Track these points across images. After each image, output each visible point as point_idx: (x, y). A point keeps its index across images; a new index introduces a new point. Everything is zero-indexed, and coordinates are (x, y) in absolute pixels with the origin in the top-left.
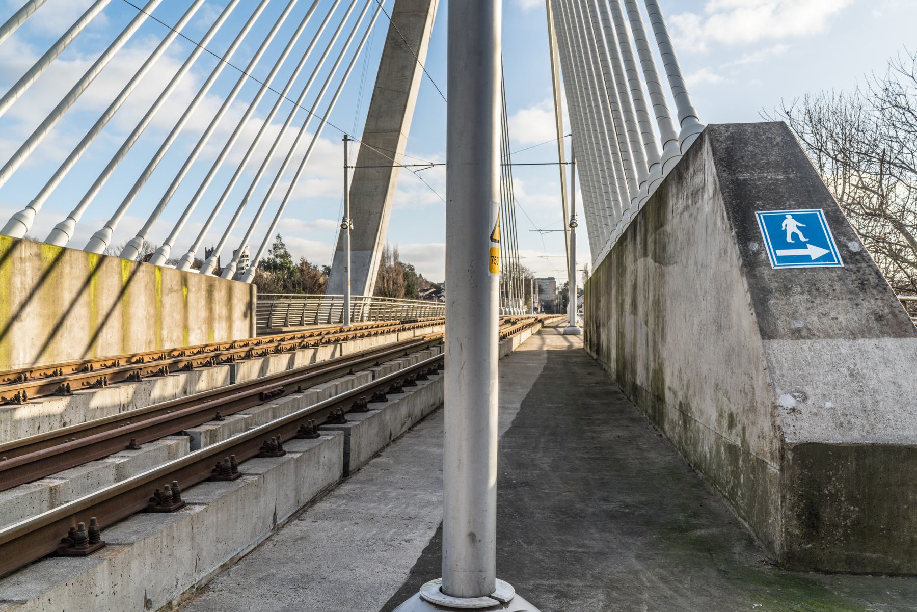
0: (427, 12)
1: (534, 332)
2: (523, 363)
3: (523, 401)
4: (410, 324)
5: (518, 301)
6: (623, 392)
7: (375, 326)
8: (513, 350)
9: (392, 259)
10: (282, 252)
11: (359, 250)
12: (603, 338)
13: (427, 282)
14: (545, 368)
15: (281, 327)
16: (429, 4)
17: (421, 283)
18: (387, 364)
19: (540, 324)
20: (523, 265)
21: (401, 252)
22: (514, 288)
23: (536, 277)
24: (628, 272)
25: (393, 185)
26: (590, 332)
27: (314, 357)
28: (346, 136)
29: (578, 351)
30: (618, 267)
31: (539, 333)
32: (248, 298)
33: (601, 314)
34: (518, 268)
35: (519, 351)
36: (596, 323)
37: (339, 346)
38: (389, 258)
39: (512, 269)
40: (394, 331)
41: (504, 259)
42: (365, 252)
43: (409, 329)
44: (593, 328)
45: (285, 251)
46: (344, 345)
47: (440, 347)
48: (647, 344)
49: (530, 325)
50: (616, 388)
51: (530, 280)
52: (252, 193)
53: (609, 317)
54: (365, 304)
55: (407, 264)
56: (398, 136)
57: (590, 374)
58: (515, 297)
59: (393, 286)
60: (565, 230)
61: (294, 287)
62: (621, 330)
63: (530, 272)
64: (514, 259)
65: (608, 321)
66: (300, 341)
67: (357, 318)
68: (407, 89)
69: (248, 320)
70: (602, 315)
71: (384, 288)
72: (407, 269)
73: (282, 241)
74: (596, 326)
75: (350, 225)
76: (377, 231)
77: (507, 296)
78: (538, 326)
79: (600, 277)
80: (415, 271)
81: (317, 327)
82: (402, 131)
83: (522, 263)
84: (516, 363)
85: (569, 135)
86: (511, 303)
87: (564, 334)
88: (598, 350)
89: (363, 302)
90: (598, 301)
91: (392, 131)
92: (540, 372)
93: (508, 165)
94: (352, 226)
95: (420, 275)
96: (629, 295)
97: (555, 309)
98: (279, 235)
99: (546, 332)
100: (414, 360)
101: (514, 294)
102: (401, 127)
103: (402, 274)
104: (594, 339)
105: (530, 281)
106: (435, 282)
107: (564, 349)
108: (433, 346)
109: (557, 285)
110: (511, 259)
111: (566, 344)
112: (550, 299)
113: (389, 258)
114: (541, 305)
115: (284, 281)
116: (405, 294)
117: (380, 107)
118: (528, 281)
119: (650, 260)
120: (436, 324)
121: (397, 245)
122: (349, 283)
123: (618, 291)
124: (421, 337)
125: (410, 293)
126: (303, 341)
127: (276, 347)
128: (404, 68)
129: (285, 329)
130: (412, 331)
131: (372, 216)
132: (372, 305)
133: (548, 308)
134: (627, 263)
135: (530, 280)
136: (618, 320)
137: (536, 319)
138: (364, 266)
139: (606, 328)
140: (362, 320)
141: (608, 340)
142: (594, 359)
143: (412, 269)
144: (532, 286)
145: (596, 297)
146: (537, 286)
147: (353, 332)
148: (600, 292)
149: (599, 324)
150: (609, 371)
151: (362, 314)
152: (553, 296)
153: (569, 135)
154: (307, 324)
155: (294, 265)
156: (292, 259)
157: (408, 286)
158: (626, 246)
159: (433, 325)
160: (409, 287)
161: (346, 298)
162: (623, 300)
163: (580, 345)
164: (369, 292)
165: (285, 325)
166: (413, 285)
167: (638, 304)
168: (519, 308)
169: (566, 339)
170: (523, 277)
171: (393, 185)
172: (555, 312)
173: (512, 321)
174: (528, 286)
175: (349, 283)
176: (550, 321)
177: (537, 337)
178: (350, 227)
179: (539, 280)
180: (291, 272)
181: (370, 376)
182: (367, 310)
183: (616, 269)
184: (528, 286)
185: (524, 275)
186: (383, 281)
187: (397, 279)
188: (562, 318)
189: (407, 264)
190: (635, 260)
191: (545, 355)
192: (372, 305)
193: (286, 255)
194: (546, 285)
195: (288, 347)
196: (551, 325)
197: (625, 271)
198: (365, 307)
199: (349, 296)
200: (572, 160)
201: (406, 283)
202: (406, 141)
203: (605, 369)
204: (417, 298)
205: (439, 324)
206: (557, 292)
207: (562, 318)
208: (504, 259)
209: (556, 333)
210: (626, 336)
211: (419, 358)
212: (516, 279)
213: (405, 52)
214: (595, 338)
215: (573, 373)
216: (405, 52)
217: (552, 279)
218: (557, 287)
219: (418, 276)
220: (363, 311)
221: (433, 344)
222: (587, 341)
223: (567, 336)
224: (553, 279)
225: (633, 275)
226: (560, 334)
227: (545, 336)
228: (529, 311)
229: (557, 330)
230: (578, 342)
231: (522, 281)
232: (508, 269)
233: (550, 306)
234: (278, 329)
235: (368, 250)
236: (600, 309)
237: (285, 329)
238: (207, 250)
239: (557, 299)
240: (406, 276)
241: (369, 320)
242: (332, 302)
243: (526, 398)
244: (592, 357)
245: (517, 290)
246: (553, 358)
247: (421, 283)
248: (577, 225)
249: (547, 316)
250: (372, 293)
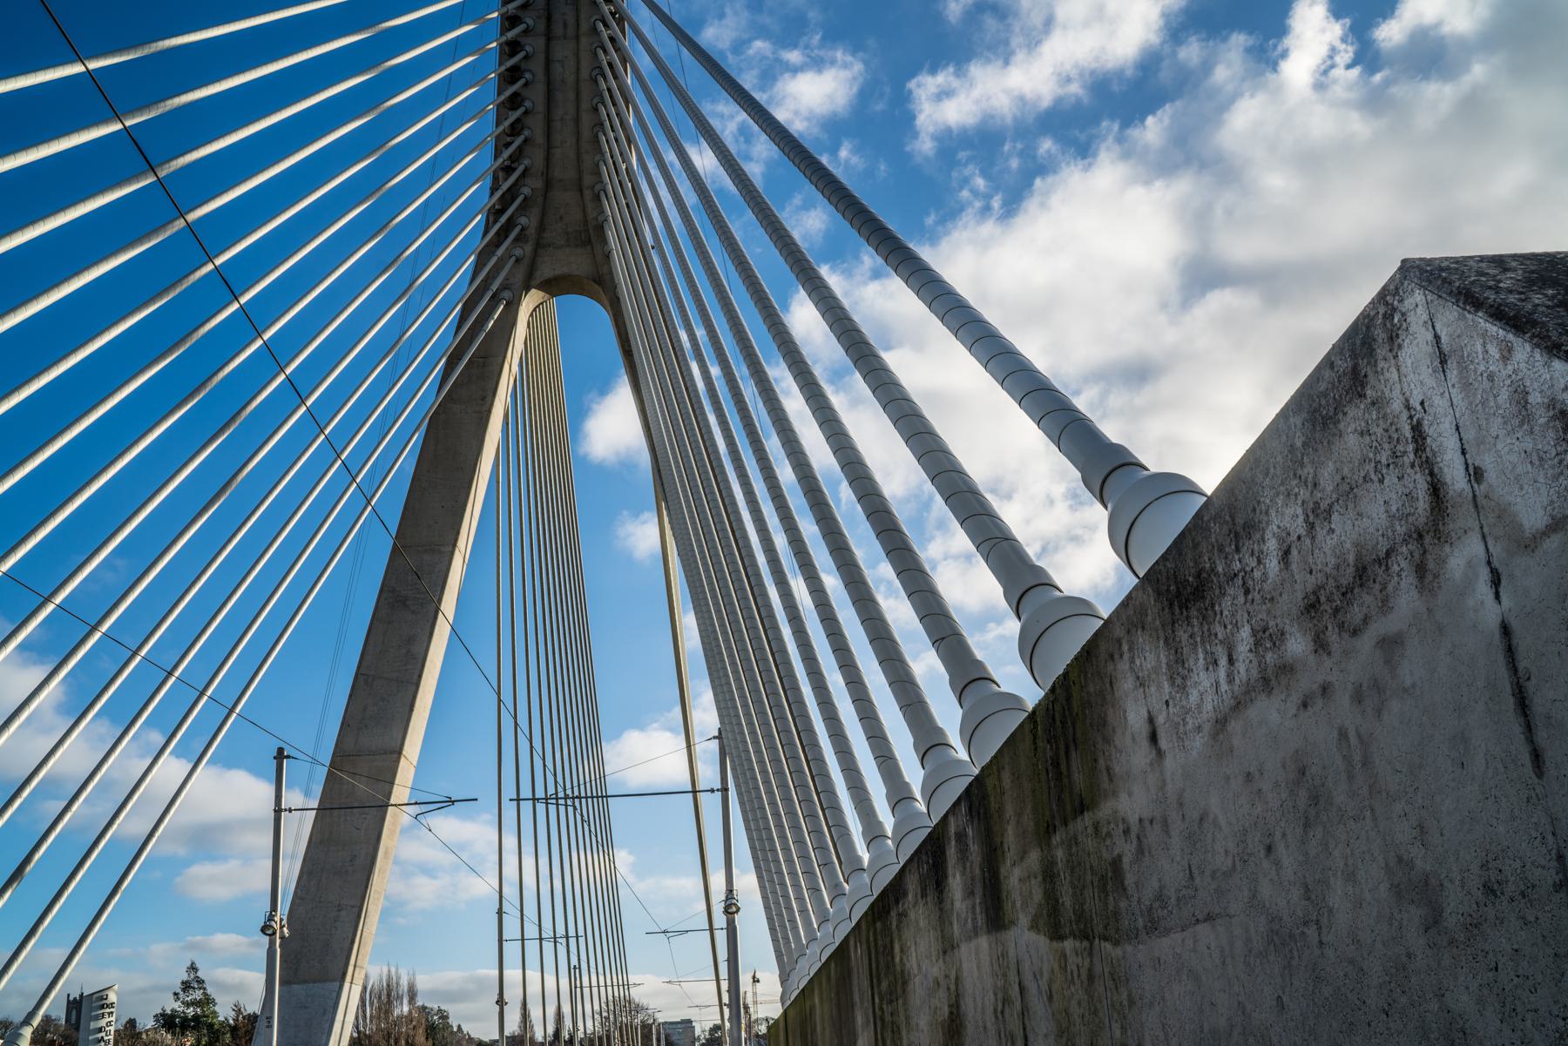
9: (405, 1001)
10: (198, 995)
20: (637, 1000)
23: (661, 1020)
24: (918, 988)
25: (386, 853)
28: (280, 750)
30: (875, 979)
34: (630, 1006)
39: (618, 1008)
41: (603, 989)
45: (205, 994)
51: (650, 1026)
55: (436, 1007)
56: (398, 761)
60: (711, 930)
63: (650, 1012)
64: (616, 988)
72: (435, 1018)
75: (282, 927)
76: (353, 942)
79: (812, 1008)
80: (450, 1021)
82: (404, 753)
83: (637, 994)
91: (385, 753)
94: (285, 930)
95: (459, 1026)
98: (193, 963)
103: (424, 1026)
105: (651, 1027)
109: (698, 1032)
110: (609, 989)
113: (400, 998)
117: (365, 709)
118: (646, 1028)
119: (1026, 941)
121: (414, 975)
131: (343, 913)
135: (650, 1026)
138: (324, 1013)
143: (444, 1016)
144: (654, 1037)
146: (663, 1037)
153: (715, 738)
155: (221, 1018)
158: (902, 915)
170: (638, 1021)
171: (386, 853)
178: (282, 932)
179: (667, 1026)
183: (866, 984)
187: (414, 1036)
189: (436, 1007)
190: (948, 947)
193: (207, 1001)
197: (905, 983)
200: (722, 783)
202: (412, 771)
208: (603, 989)
212: (626, 1025)
213: (413, 612)
217: (687, 1023)
218: (696, 1035)
219: (455, 1029)
224: (690, 1021)
225: (942, 993)
231: (636, 1029)
235: (333, 980)
238: (71, 998)
248: (738, 909)
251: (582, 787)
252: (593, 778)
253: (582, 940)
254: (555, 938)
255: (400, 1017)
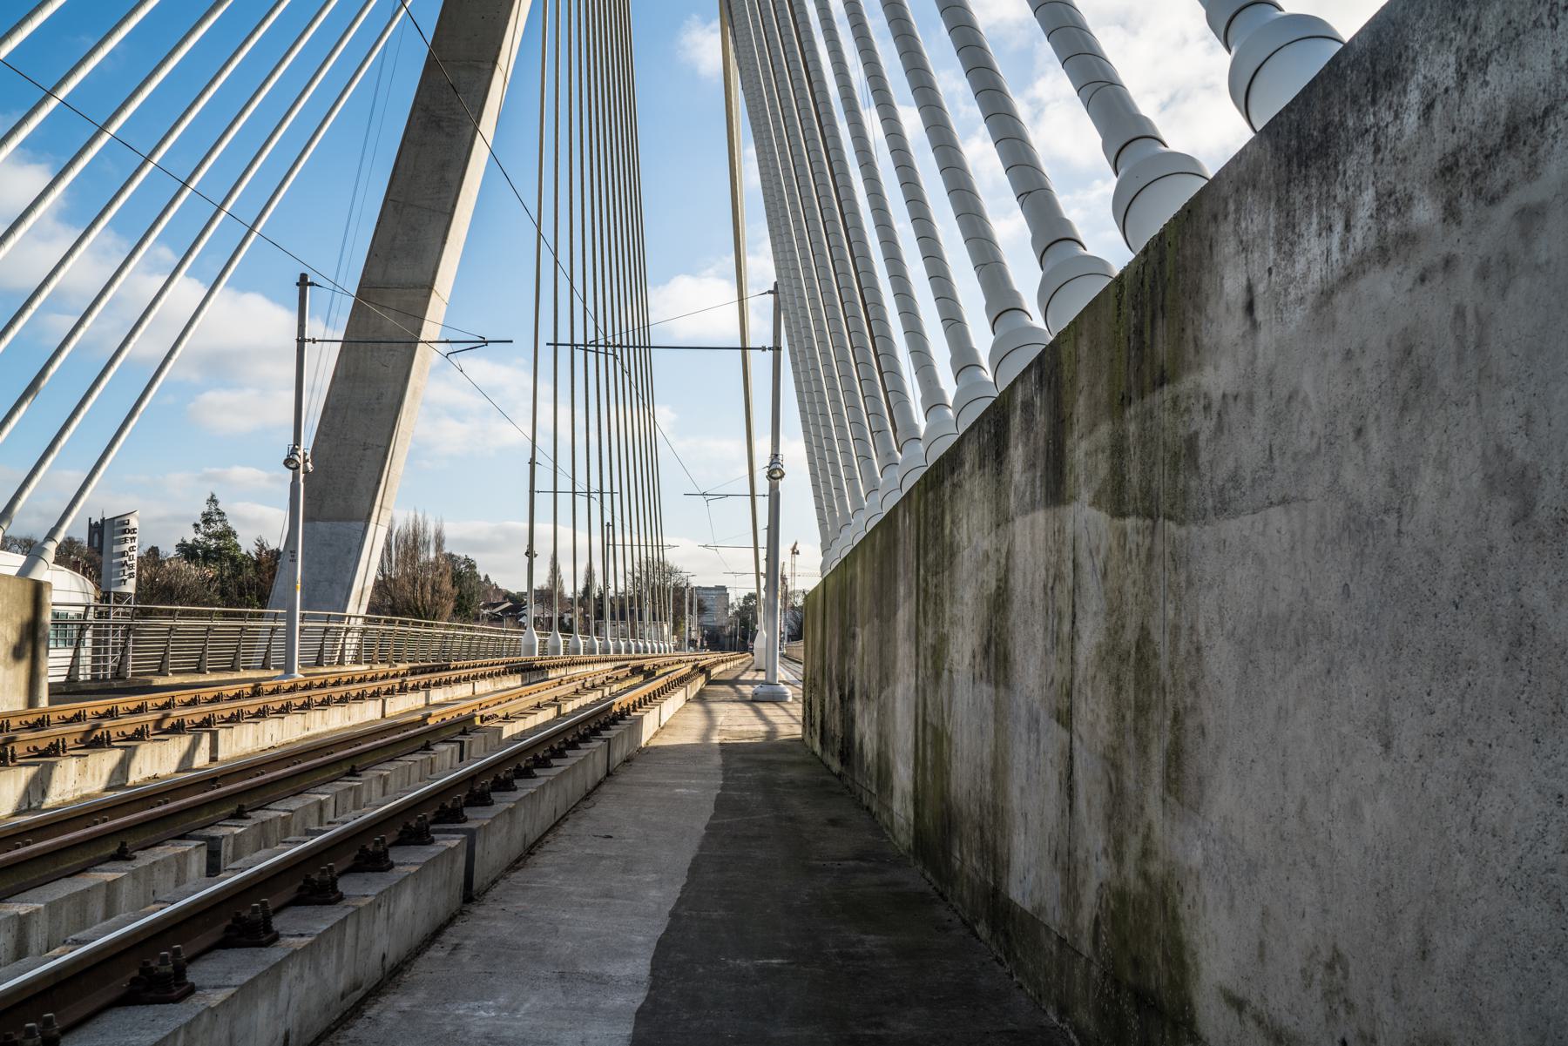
0: (495, 62)
1: (691, 696)
2: (666, 785)
3: (660, 942)
4: (428, 676)
5: (662, 627)
6: (941, 895)
7: (369, 676)
8: (643, 744)
10: (218, 527)
11: (339, 520)
12: (866, 729)
13: (498, 590)
14: (721, 804)
15: (150, 677)
16: (500, 48)
17: (485, 591)
18: (277, 812)
19: (704, 676)
20: (671, 563)
21: (449, 533)
22: (654, 603)
26: (823, 706)
27: (123, 767)
28: (304, 277)
29: (790, 746)
30: (921, 549)
31: (701, 697)
32: (27, 613)
33: (857, 667)
35: (656, 748)
36: (841, 688)
37: (206, 739)
38: (426, 544)
39: (651, 569)
40: (375, 695)
42: (352, 524)
43: (415, 688)
44: (832, 698)
46: (222, 733)
47: (462, 743)
48: (1070, 789)
49: (682, 681)
50: (915, 878)
51: (682, 591)
52: (52, 371)
53: (886, 678)
54: (348, 630)
55: (463, 555)
56: (428, 297)
57: (833, 822)
58: (654, 619)
59: (432, 596)
61: (241, 594)
62: (932, 718)
63: (684, 575)
65: (881, 690)
66: (158, 716)
67: (331, 658)
68: (449, 206)
69: (23, 668)
70: (861, 668)
71: (415, 599)
72: (462, 566)
73: (219, 506)
74: (842, 697)
75: (305, 461)
76: (379, 483)
77: (641, 618)
78: (700, 682)
79: (854, 578)
80: (478, 570)
81: (321, 670)
82: (435, 288)
83: (672, 558)
84: (646, 785)
85: (770, 292)
86: (647, 631)
87: (753, 701)
88: (848, 751)
89: (345, 625)
90: (847, 636)
92: (706, 818)
93: (640, 347)
94: (309, 465)
95: (487, 577)
96: (968, 624)
97: (727, 642)
98: (213, 496)
99: (715, 694)
100: (376, 788)
101: (654, 614)
102: (434, 278)
103: (450, 574)
104: (835, 723)
105: (684, 593)
106: (514, 590)
107: (759, 740)
108: (445, 741)
109: (732, 599)
111: (762, 728)
112: (719, 624)
114: (703, 635)
115: (222, 581)
116: (454, 611)
117: (394, 239)
118: (679, 592)
120: (483, 677)
121: (442, 521)
122: (299, 585)
123: (920, 613)
124: (418, 717)
125: (463, 609)
126: (166, 716)
127: (88, 733)
128: (444, 166)
129: (159, 681)
130: (422, 694)
131: (369, 452)
132: (364, 632)
133: (715, 640)
134: (962, 535)
136: (920, 691)
137: (695, 667)
139: (874, 706)
140: (341, 662)
141: (882, 737)
142: (834, 774)
143: (471, 565)
144: (687, 601)
145: (842, 624)
146: (695, 601)
147: (358, 686)
148: (853, 615)
149: (852, 692)
150: (885, 816)
151: (343, 650)
152: (724, 619)
153: (770, 292)
154: (211, 670)
155: (244, 552)
156: (239, 541)
157: (461, 596)
158: (956, 486)
159: (475, 678)
160: (463, 597)
161: (290, 618)
162: (942, 640)
163: (792, 731)
164: (357, 606)
165: (161, 672)
166: (472, 594)
167: (1017, 653)
168: (662, 639)
169: (758, 713)
171: (415, 393)
172: (727, 647)
173: (646, 668)
174: (679, 600)
175: (299, 585)
176: (721, 668)
177: (696, 707)
178: (305, 466)
180: (237, 566)
181: (197, 862)
182: (352, 642)
184: (679, 600)
185: (674, 580)
186: (414, 586)
188: (741, 661)
191: (717, 760)
192: (364, 632)
193: (228, 533)
194: (712, 599)
195: (227, 715)
196: (723, 677)
197: (953, 555)
198: (350, 635)
199: (298, 612)
200: (775, 342)
201: (456, 591)
202: (444, 308)
203: (868, 809)
204: (477, 619)
205: (490, 675)
206: (730, 612)
207: (741, 661)
209: (735, 697)
210: (956, 738)
211: (392, 781)
212: (659, 588)
214: (838, 723)
215: (791, 819)
216: (448, 134)
219: (482, 579)
220: (343, 645)
221: (444, 734)
222: (812, 725)
223: (761, 706)
224: (724, 588)
225: (991, 567)
226: (743, 700)
227: (714, 706)
228: (680, 646)
229: (737, 691)
230: (788, 722)
231: (669, 592)
232: (644, 568)
233: (718, 637)
234: (144, 681)
235: (359, 520)
236: (852, 655)
237: (159, 681)
238: (93, 522)
239: (731, 624)
240: (458, 578)
241: (357, 662)
242: (273, 624)
243: (668, 930)
244: (828, 767)
245: (660, 607)
246: (736, 771)
247: (485, 591)
248: (783, 475)
249: (718, 656)
250: (363, 611)
251: (624, 336)
252: (636, 327)
253: (617, 497)
254: (589, 492)
255: (427, 564)
